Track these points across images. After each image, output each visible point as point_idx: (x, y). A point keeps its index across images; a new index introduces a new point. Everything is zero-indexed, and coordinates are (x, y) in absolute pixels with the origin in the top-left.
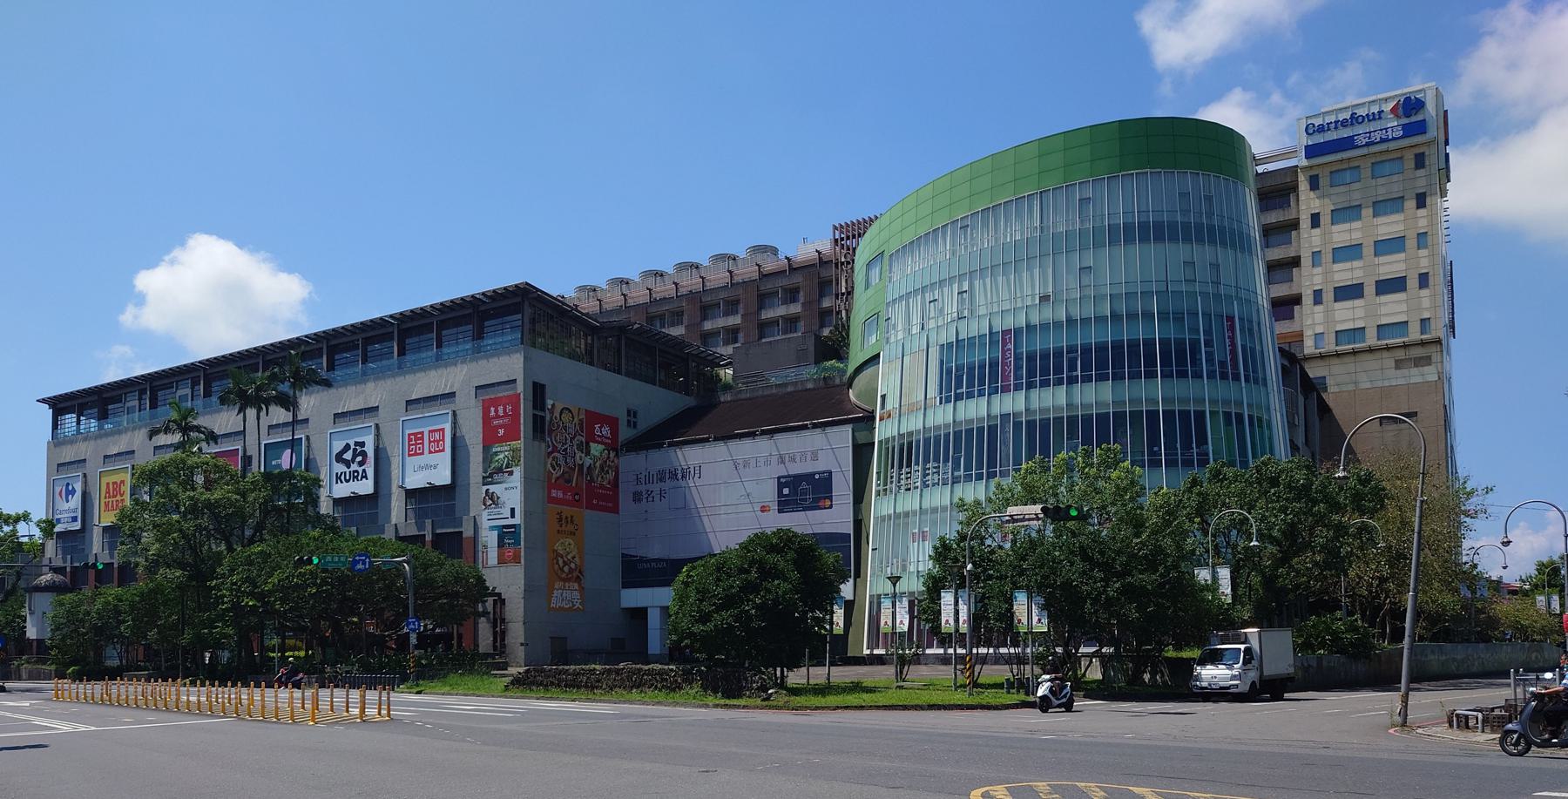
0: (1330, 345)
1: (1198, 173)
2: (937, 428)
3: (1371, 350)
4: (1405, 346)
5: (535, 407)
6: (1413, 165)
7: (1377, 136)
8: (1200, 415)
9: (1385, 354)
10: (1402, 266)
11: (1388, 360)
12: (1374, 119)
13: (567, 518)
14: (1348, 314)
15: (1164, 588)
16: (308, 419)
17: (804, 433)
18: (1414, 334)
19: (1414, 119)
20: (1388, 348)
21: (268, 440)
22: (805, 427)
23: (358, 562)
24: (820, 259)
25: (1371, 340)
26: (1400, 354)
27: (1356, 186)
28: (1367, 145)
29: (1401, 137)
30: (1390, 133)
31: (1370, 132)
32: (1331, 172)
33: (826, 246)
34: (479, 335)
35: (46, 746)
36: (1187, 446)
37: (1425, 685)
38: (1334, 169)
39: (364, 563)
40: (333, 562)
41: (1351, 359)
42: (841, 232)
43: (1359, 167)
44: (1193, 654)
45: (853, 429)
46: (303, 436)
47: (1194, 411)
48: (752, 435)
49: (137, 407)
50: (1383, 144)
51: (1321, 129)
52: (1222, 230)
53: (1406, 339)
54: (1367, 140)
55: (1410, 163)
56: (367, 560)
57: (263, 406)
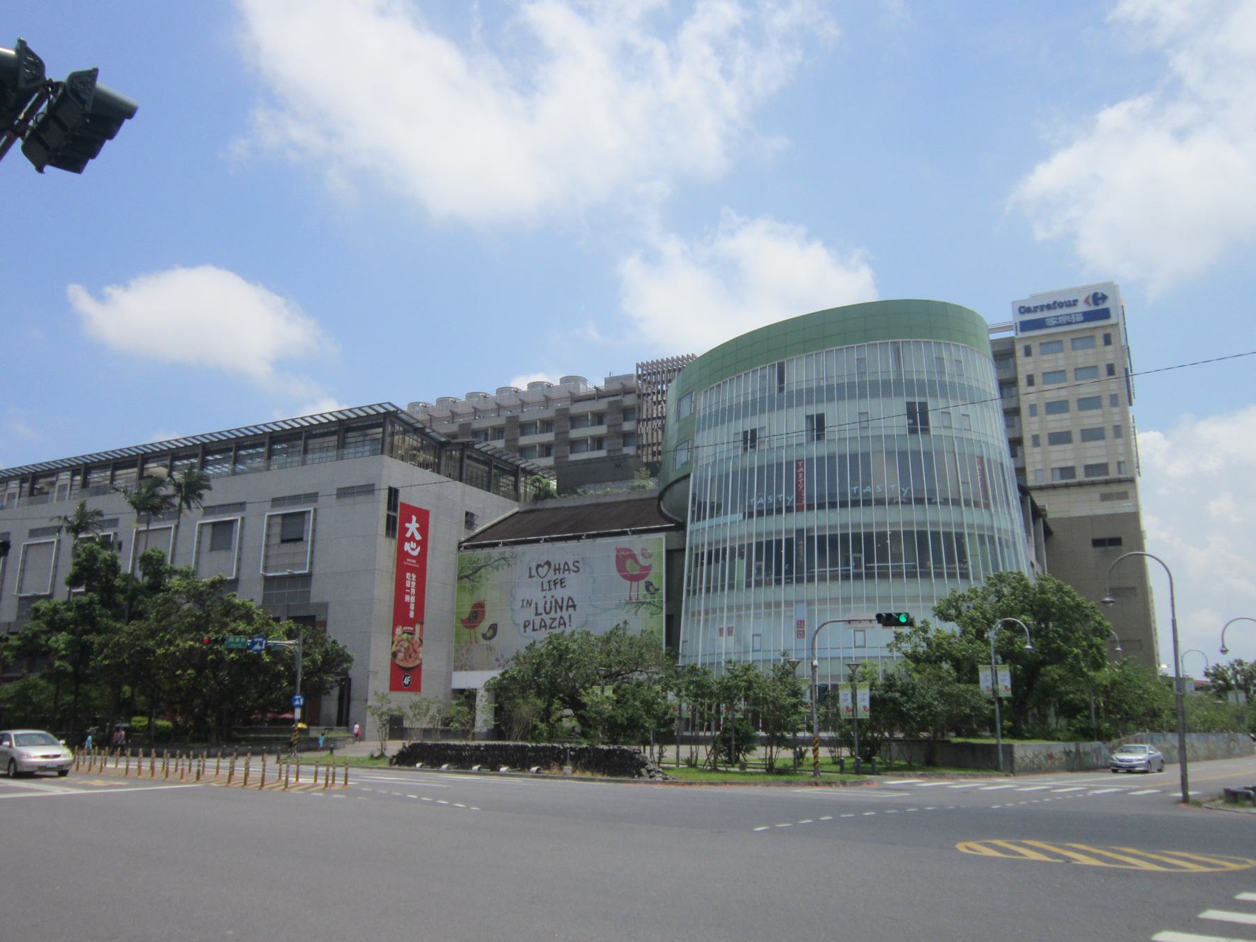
0: (1047, 480)
1: (930, 342)
2: (769, 533)
3: (1080, 485)
4: (1107, 483)
5: (389, 509)
6: (1102, 343)
7: (1064, 319)
8: (960, 537)
9: (1093, 489)
10: (1100, 420)
11: (1096, 493)
14: (1062, 456)
16: (117, 520)
17: (536, 546)
18: (1113, 474)
20: (1093, 484)
21: (271, 511)
22: (537, 541)
23: (256, 643)
25: (1080, 476)
26: (1106, 489)
28: (1056, 325)
29: (1083, 322)
30: (1073, 318)
32: (1073, 340)
34: (342, 445)
36: (950, 560)
37: (889, 773)
38: (1076, 337)
39: (261, 644)
40: (234, 642)
41: (1063, 491)
42: (643, 370)
44: (1091, 746)
45: (666, 537)
46: (312, 509)
47: (943, 533)
48: (578, 538)
49: (17, 495)
51: (1027, 310)
52: (952, 385)
53: (1106, 477)
55: (1100, 340)
56: (264, 642)
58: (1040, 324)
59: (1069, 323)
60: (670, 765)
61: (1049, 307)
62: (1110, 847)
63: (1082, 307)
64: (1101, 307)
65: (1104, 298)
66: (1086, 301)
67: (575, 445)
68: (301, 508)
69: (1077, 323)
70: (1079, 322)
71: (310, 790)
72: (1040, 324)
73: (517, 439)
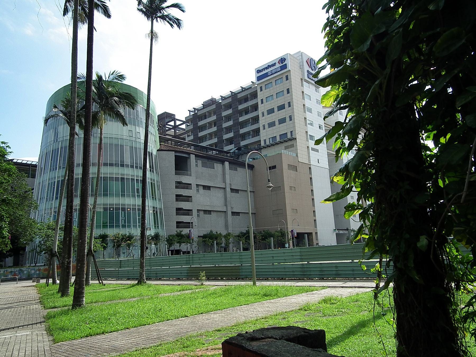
6: (285, 80)
12: (274, 66)
13: (188, 199)
15: (452, 294)
16: (275, 166)
18: (289, 136)
19: (284, 64)
24: (232, 94)
27: (271, 88)
28: (271, 75)
31: (272, 70)
33: (267, 66)
35: (96, 31)
38: (266, 84)
43: (272, 82)
50: (276, 74)
54: (271, 73)
57: (421, 107)
58: (266, 75)
59: (275, 73)
60: (42, 177)
61: (267, 68)
62: (396, 309)
63: (278, 65)
64: (284, 64)
65: (285, 59)
66: (279, 62)
67: (203, 139)
68: (252, 238)
69: (278, 72)
70: (280, 71)
71: (64, 202)
72: (266, 75)
73: (239, 119)
